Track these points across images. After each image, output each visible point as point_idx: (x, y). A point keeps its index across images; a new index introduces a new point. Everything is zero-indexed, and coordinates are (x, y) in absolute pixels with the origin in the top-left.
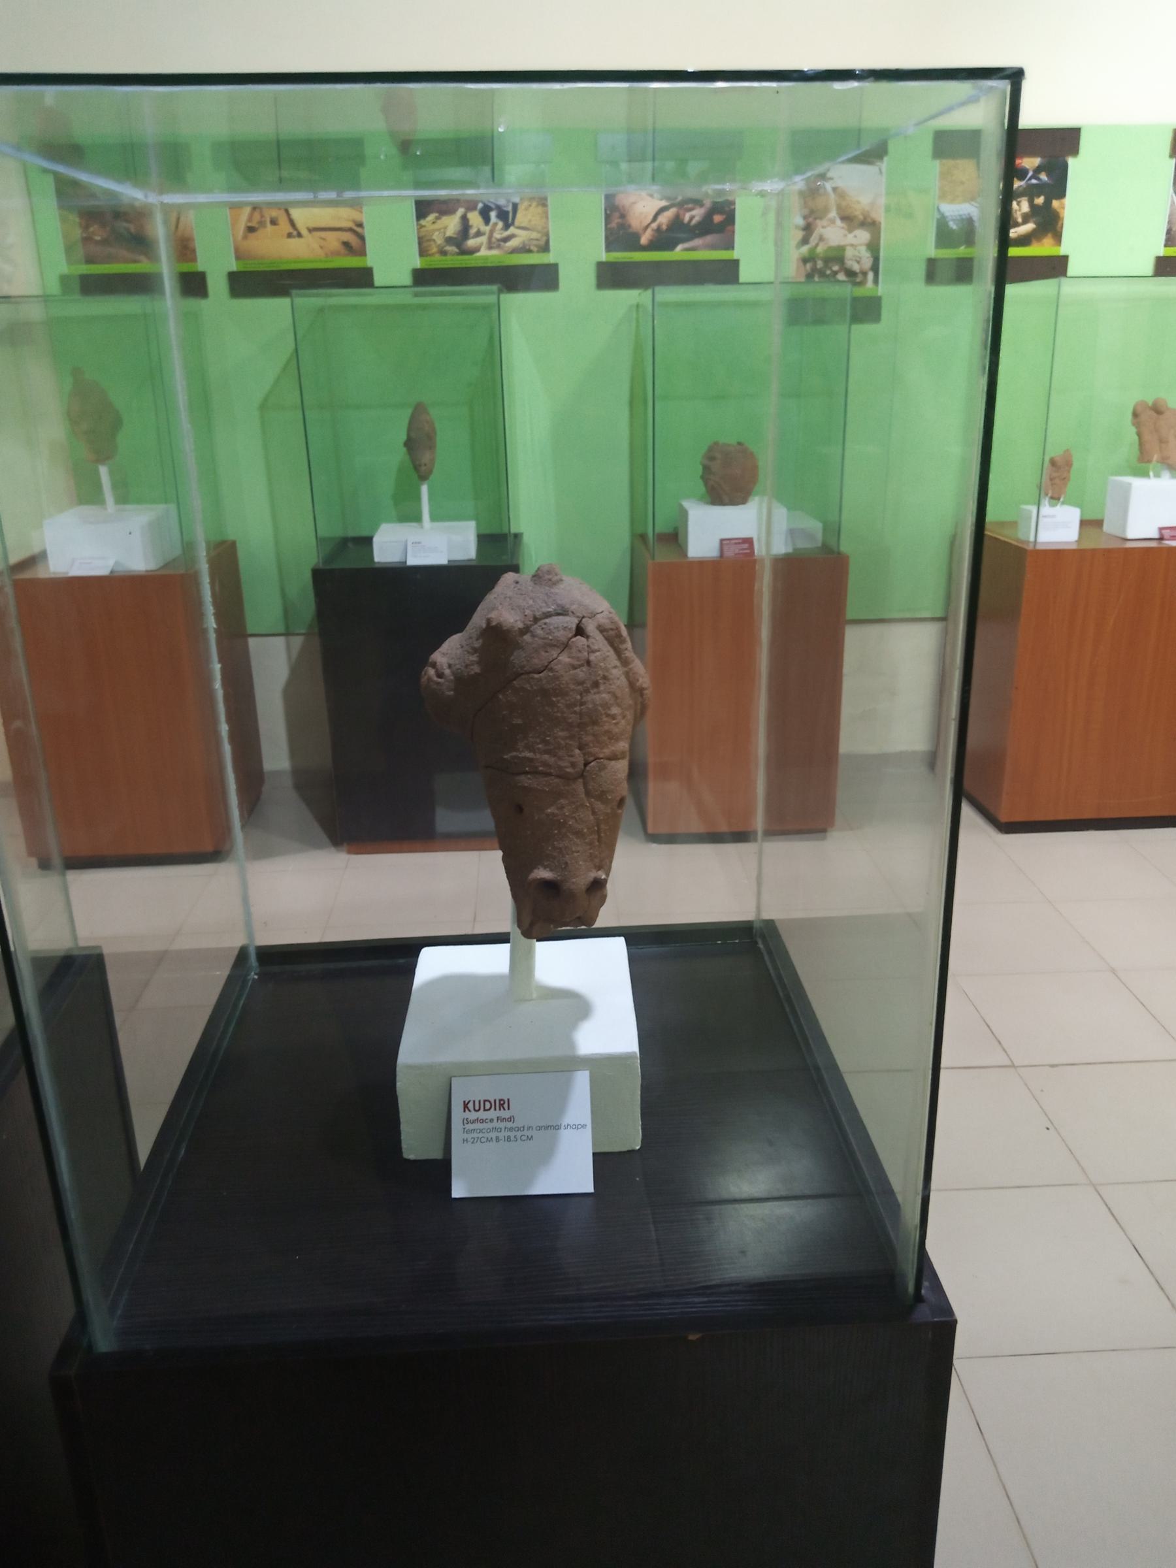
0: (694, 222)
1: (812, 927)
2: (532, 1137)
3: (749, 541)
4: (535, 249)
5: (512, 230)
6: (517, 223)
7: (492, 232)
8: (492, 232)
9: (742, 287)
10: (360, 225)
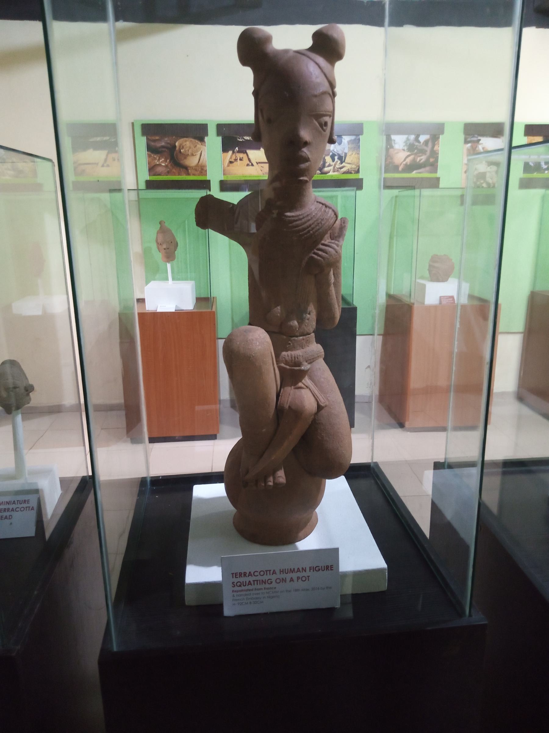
0: (422, 161)
2: (333, 570)
3: (452, 297)
5: (344, 164)
7: (335, 165)
8: (335, 165)
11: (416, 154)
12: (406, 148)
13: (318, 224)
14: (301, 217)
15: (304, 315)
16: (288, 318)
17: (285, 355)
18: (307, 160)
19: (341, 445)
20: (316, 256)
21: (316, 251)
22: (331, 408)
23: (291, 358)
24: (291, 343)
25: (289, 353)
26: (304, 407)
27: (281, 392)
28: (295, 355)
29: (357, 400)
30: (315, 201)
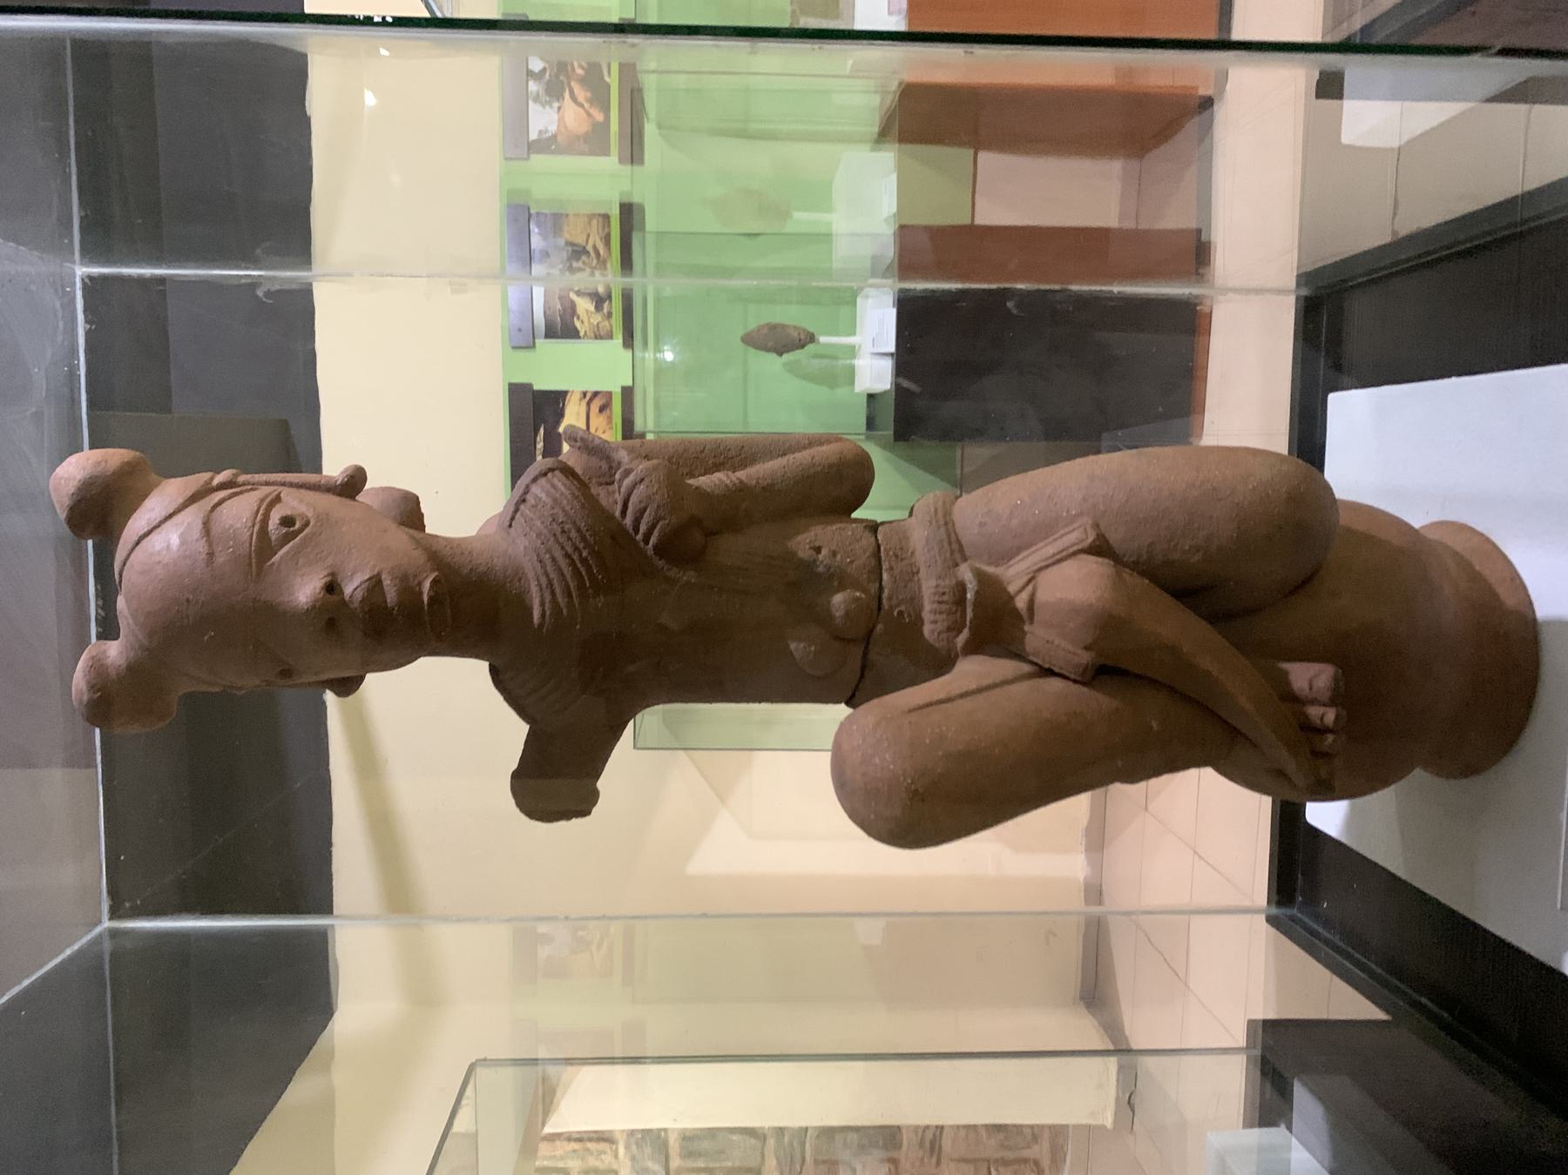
1: (1308, 232)
4: (606, 230)
5: (589, 248)
6: (584, 243)
9: (638, 381)
10: (585, 394)
11: (569, 78)
12: (556, 105)
13: (563, 532)
14: (544, 581)
15: (821, 569)
16: (823, 618)
17: (933, 631)
18: (375, 583)
19: (1228, 492)
20: (653, 540)
21: (639, 537)
22: (1105, 511)
23: (941, 613)
24: (899, 609)
25: (927, 616)
26: (1091, 605)
27: (1040, 662)
28: (933, 602)
29: (1129, 224)
30: (509, 533)
